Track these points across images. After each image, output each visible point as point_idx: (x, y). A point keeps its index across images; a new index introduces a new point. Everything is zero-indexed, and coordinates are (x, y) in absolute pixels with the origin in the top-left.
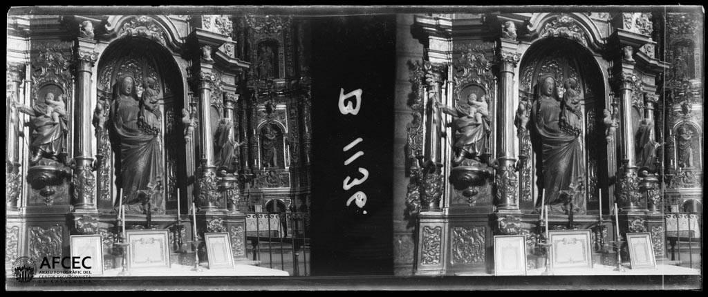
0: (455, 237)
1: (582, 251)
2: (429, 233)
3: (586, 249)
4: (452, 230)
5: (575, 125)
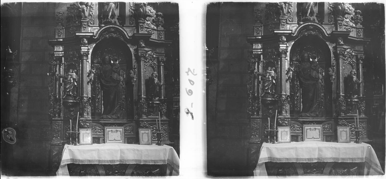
0: (264, 126)
1: (319, 133)
2: (254, 124)
3: (320, 133)
4: (263, 124)
5: (315, 76)
